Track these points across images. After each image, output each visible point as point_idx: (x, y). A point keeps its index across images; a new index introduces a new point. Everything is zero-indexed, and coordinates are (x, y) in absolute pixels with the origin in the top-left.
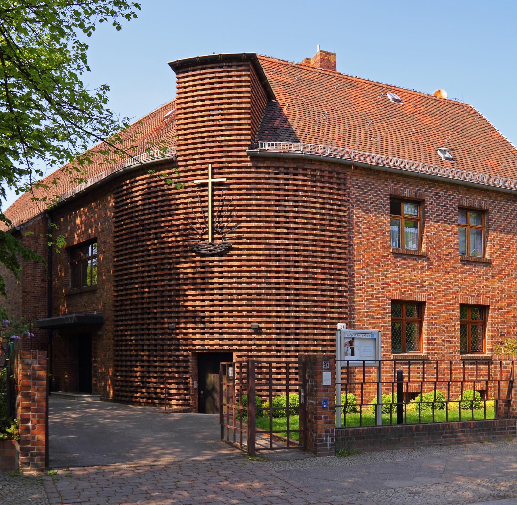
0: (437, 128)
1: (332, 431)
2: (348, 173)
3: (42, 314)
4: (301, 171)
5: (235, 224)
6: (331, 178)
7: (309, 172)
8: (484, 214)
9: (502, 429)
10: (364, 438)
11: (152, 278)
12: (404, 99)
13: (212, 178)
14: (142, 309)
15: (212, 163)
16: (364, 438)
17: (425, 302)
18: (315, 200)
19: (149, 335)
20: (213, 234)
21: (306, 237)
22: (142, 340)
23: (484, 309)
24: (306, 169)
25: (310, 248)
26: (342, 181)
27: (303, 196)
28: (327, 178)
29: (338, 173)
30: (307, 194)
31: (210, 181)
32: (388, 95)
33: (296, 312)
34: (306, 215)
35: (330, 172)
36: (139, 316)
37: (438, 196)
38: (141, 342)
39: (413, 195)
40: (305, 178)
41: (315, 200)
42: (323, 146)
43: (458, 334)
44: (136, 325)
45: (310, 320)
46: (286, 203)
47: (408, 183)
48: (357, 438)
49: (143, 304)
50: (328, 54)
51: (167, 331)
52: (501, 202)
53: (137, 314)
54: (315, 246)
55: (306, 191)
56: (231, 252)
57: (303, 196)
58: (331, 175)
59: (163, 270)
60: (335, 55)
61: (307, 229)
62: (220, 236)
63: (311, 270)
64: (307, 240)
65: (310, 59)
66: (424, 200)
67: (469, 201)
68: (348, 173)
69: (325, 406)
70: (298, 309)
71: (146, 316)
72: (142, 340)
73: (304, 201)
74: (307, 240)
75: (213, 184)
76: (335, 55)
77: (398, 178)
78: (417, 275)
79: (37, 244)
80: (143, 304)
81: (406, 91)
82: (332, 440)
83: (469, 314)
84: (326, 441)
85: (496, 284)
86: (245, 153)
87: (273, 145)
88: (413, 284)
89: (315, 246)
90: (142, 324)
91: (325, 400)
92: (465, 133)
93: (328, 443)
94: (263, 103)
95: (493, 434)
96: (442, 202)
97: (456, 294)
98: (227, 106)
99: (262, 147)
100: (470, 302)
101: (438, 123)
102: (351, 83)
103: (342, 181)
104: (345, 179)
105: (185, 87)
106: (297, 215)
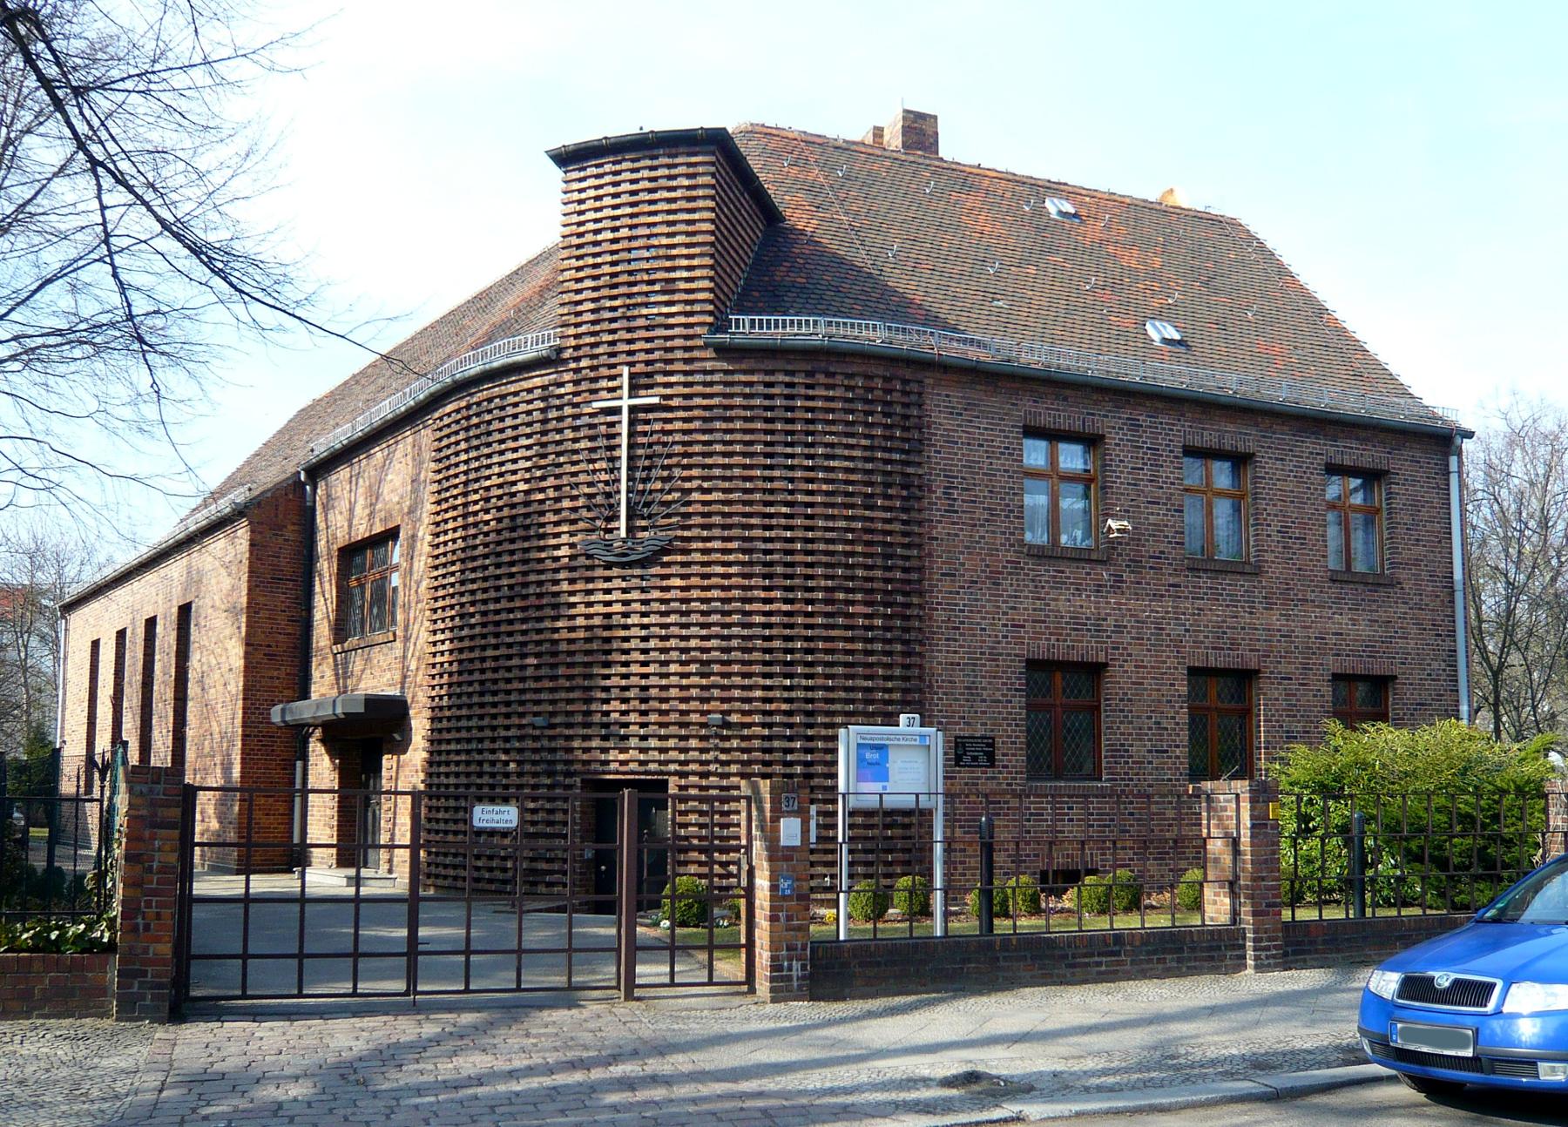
0: (1154, 275)
1: (804, 948)
2: (927, 381)
3: (286, 693)
4: (821, 378)
5: (676, 495)
6: (890, 391)
7: (838, 380)
8: (1245, 464)
9: (1211, 949)
10: (878, 964)
11: (504, 616)
12: (1084, 212)
13: (630, 397)
14: (482, 683)
15: (631, 364)
16: (878, 964)
17: (1106, 665)
18: (852, 441)
19: (493, 740)
20: (629, 518)
21: (831, 524)
22: (480, 752)
23: (1244, 678)
24: (833, 375)
25: (840, 548)
26: (914, 398)
27: (826, 433)
28: (880, 393)
29: (905, 382)
30: (834, 428)
31: (625, 403)
32: (1048, 204)
33: (807, 688)
34: (832, 476)
35: (886, 379)
36: (476, 699)
37: (1135, 426)
38: (477, 757)
39: (1077, 426)
40: (831, 393)
41: (852, 441)
42: (803, 330)
43: (1185, 736)
44: (469, 718)
45: (838, 707)
46: (789, 450)
47: (1065, 399)
48: (861, 964)
49: (483, 671)
50: (921, 117)
51: (531, 731)
52: (1284, 436)
53: (470, 695)
54: (851, 542)
55: (833, 422)
56: (665, 559)
57: (826, 433)
58: (888, 386)
59: (525, 597)
60: (935, 117)
61: (833, 505)
62: (644, 523)
63: (841, 596)
64: (832, 529)
65: (882, 129)
66: (1103, 436)
67: (1208, 437)
68: (927, 381)
69: (788, 892)
70: (810, 682)
71: (488, 699)
72: (480, 752)
73: (827, 445)
74: (832, 529)
75: (632, 409)
76: (935, 117)
77: (1042, 389)
78: (1087, 604)
79: (280, 540)
80: (483, 671)
81: (1092, 194)
82: (804, 967)
83: (1214, 687)
84: (790, 969)
85: (1275, 619)
86: (700, 342)
87: (792, 322)
88: (1078, 623)
89: (851, 542)
90: (481, 717)
91: (786, 879)
92: (1218, 282)
93: (794, 973)
94: (751, 231)
95: (1189, 959)
96: (1145, 439)
97: (1178, 643)
98: (665, 241)
99: (737, 327)
100: (1212, 663)
101: (1158, 262)
102: (967, 179)
103: (914, 398)
104: (920, 394)
105: (581, 202)
106: (811, 474)
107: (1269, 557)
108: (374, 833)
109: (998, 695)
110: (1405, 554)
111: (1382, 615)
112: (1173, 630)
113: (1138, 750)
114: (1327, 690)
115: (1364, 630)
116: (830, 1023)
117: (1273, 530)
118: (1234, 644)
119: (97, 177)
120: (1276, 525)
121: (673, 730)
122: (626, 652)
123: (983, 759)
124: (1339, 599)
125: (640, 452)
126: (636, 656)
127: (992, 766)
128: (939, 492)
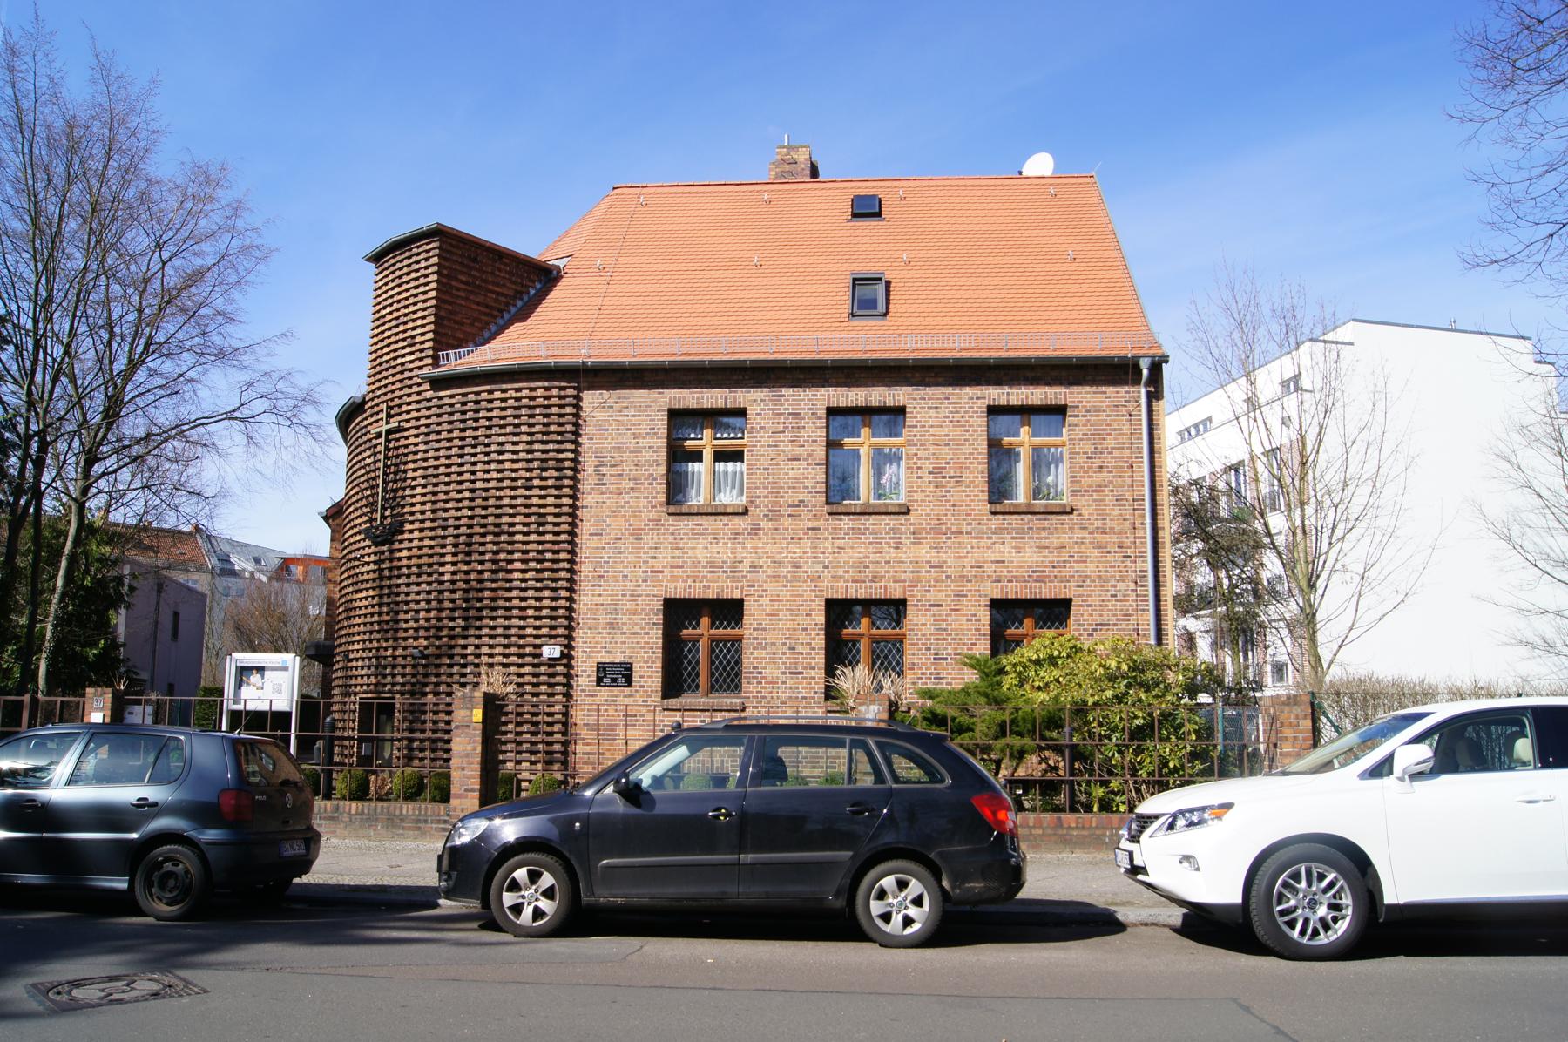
78: (724, 552)
85: (924, 552)
88: (713, 567)
107: (918, 496)
109: (637, 629)
110: (1086, 482)
112: (811, 567)
113: (772, 672)
114: (985, 616)
115: (1031, 557)
117: (924, 472)
120: (927, 467)
121: (528, 659)
122: (509, 599)
123: (621, 680)
124: (1000, 530)
125: (569, 446)
126: (516, 602)
127: (630, 685)
128: (590, 470)
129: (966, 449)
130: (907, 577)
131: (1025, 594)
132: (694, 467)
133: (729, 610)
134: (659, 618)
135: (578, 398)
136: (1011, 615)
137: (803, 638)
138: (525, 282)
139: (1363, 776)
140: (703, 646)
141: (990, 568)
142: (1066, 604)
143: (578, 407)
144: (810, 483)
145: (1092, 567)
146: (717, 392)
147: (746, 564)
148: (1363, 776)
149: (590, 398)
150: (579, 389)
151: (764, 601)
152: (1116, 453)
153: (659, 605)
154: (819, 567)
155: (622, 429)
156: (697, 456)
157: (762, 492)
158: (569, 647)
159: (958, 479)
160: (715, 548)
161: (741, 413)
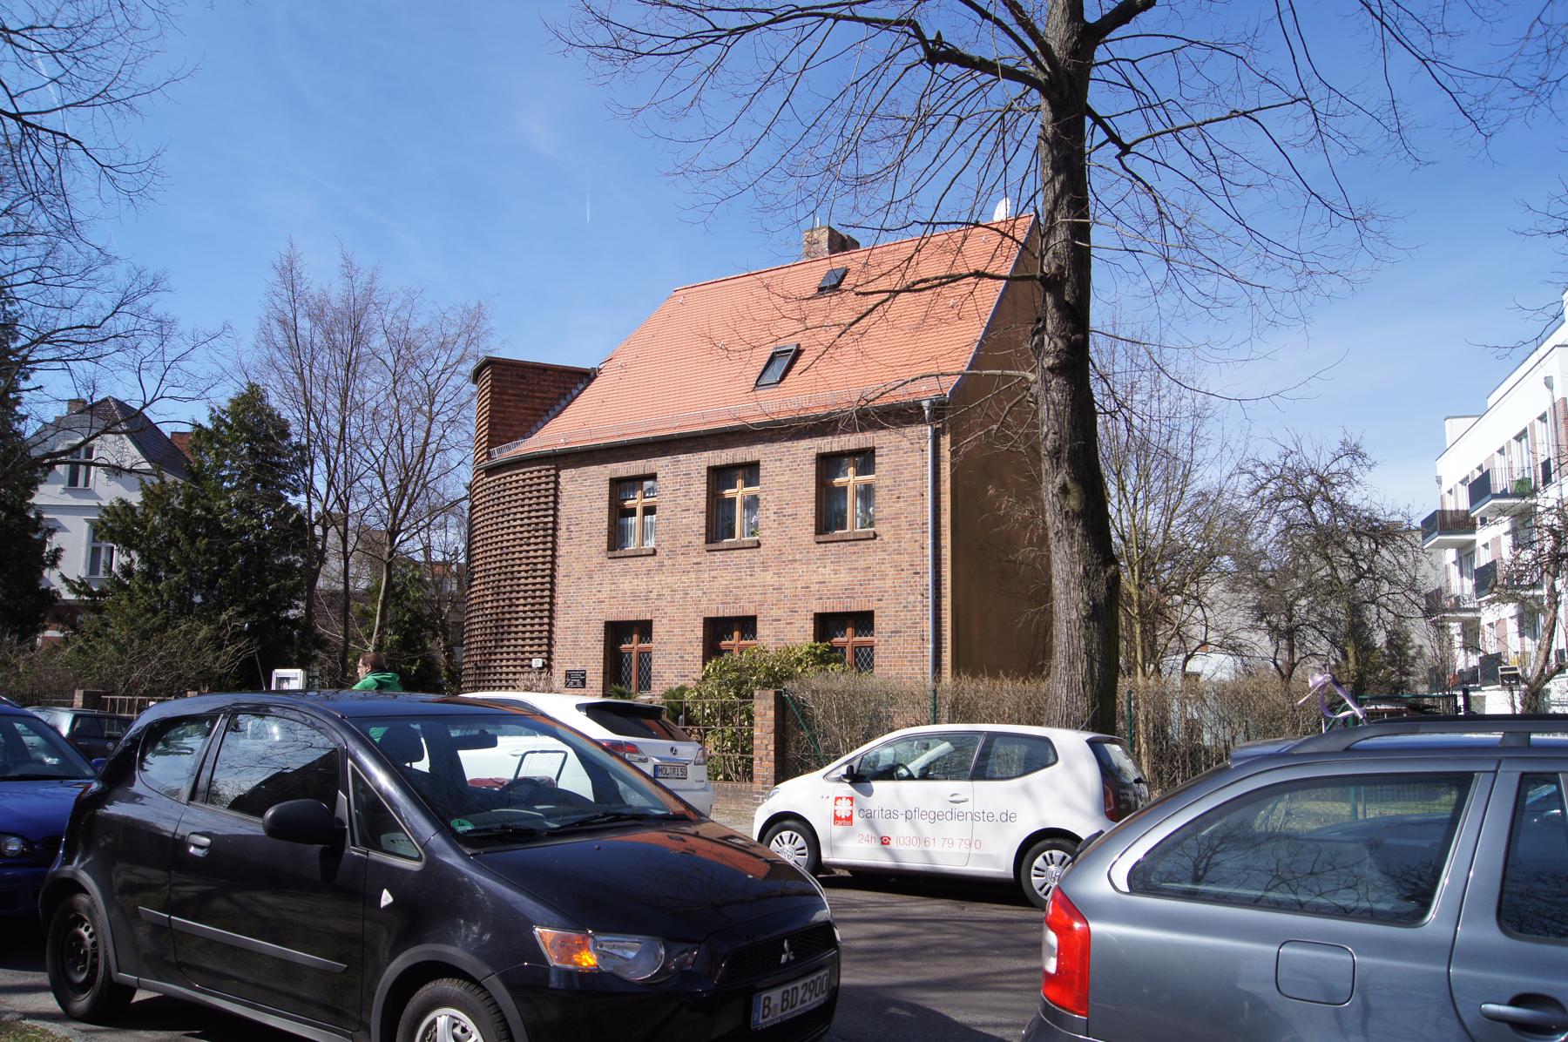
78: (641, 584)
85: (769, 578)
88: (635, 596)
108: (853, 961)
111: (861, 563)
115: (844, 577)
116: (996, 1025)
118: (737, 599)
119: (1163, 226)
124: (822, 557)
129: (801, 491)
130: (757, 598)
131: (839, 609)
132: (632, 520)
133: (644, 629)
134: (601, 637)
135: (557, 476)
136: (718, 631)
137: (690, 649)
138: (565, 384)
139: (579, 707)
140: (634, 656)
141: (814, 587)
142: (754, 619)
143: (557, 483)
144: (695, 528)
145: (889, 583)
146: (639, 462)
147: (653, 595)
148: (579, 707)
149: (565, 475)
150: (558, 470)
151: (665, 621)
152: (911, 484)
153: (601, 627)
154: (700, 593)
155: (584, 493)
156: (632, 512)
157: (665, 537)
158: (549, 659)
159: (794, 516)
160: (635, 582)
161: (653, 477)
